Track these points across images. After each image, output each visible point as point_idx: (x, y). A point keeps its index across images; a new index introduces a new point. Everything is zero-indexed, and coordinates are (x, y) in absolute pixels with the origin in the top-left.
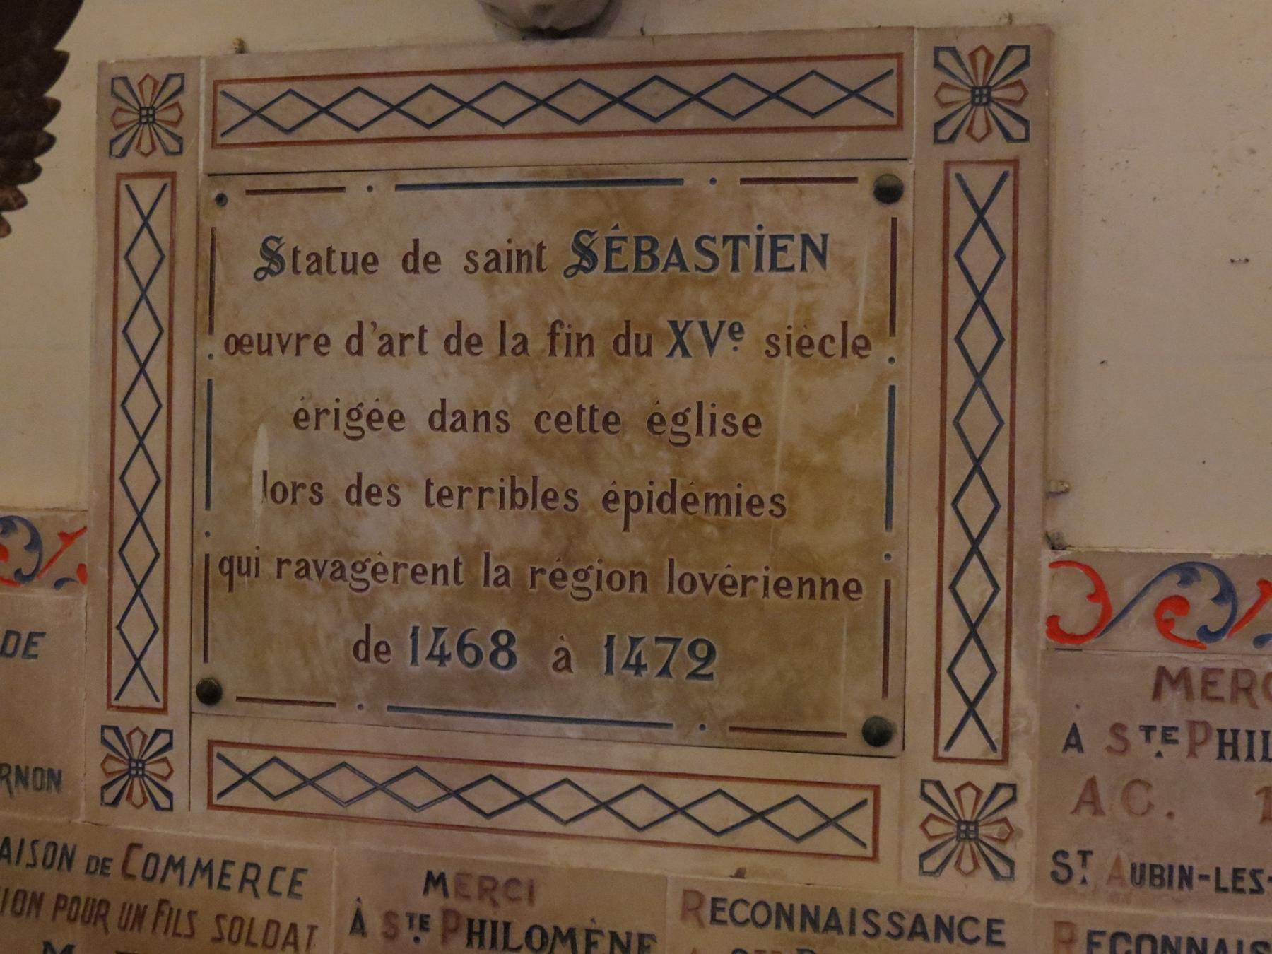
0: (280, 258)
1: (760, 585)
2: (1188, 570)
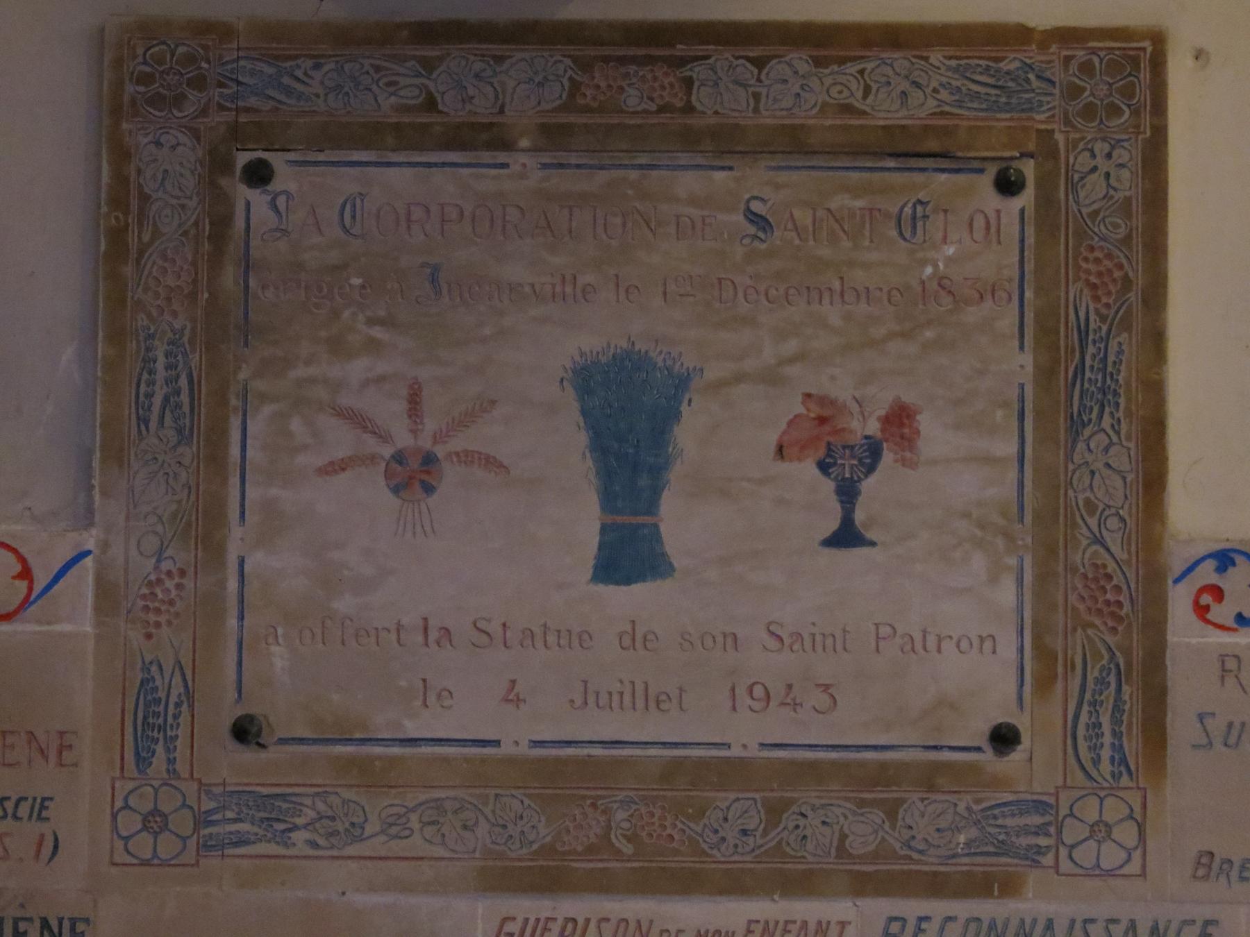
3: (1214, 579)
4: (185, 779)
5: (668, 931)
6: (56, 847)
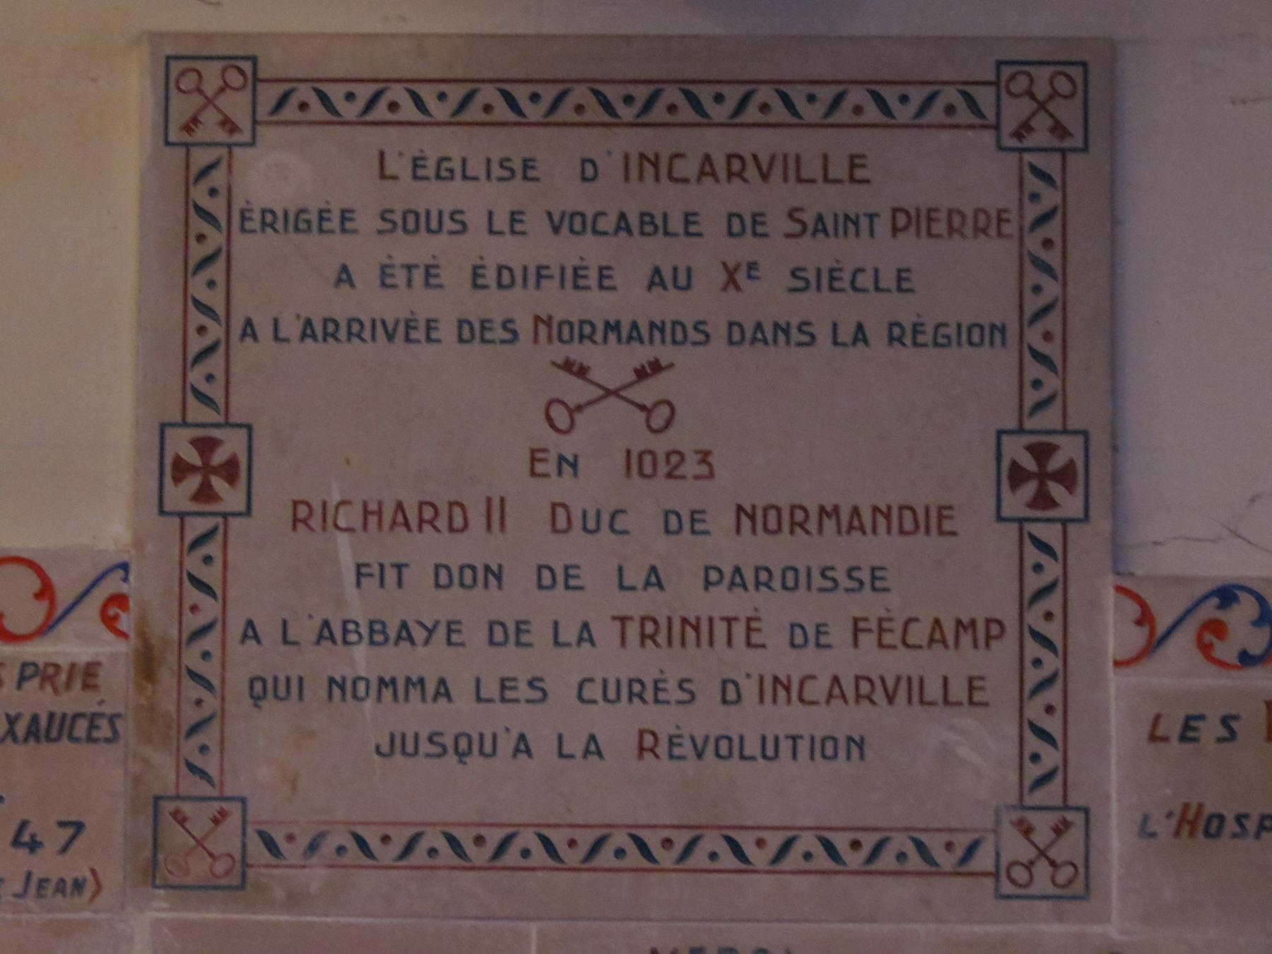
2: (1226, 595)
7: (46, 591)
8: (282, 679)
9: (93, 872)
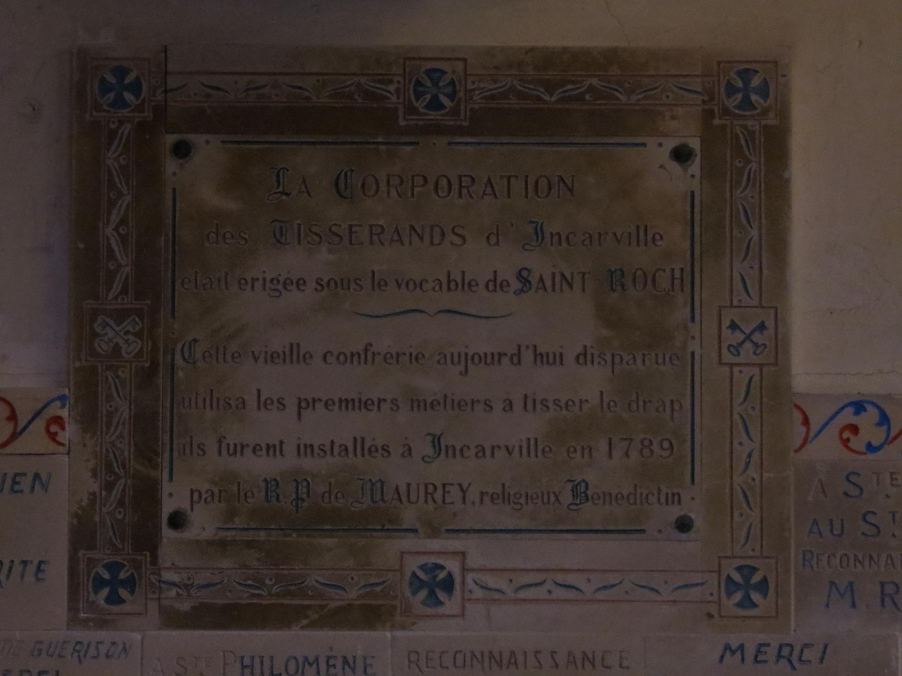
0: (530, 283)
1: (407, 358)
2: (859, 407)
3: (854, 420)
4: (465, 176)
5: (28, 671)
6: (337, 184)
7: (13, 417)
8: (357, 409)
9: (794, 668)
